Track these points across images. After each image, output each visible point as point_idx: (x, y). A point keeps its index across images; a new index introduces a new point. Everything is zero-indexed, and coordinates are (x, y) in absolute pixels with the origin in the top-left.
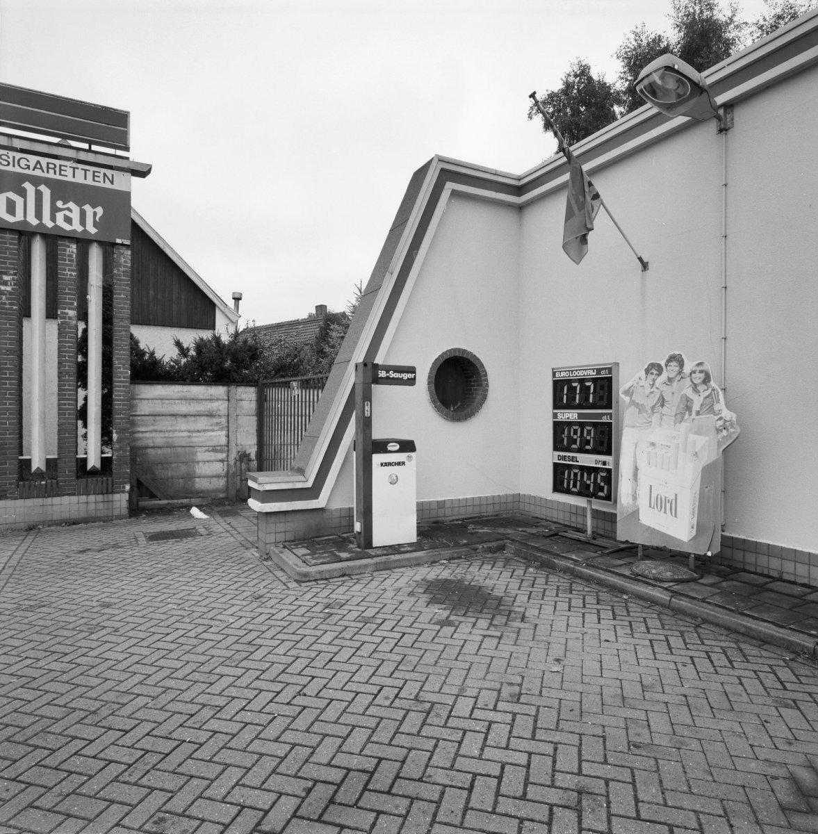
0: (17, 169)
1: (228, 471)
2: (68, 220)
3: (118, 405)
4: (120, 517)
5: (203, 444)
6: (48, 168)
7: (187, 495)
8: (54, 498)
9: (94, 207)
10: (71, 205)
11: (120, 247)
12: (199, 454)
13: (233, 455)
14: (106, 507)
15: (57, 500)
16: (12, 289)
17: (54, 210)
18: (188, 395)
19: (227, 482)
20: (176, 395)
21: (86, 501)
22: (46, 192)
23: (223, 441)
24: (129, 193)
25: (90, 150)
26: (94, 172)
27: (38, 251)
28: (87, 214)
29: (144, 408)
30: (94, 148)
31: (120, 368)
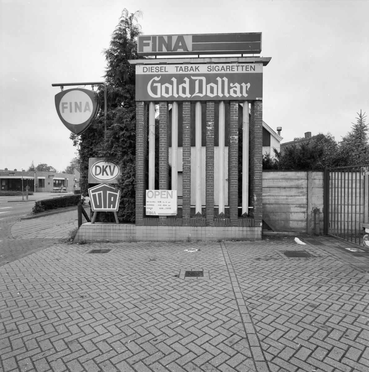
0: (215, 72)
1: (307, 218)
2: (235, 92)
3: (256, 182)
4: (258, 239)
5: (294, 203)
6: (227, 68)
7: (286, 230)
8: (229, 227)
9: (246, 84)
10: (237, 84)
11: (258, 102)
12: (292, 208)
13: (310, 210)
14: (251, 234)
15: (230, 228)
16: (212, 128)
17: (229, 88)
18: (286, 177)
19: (307, 224)
20: (280, 177)
21: (242, 230)
22: (225, 79)
23: (305, 201)
24: (262, 73)
25: (242, 57)
26: (246, 66)
27: (198, 108)
28: (243, 87)
29: (265, 184)
30: (244, 55)
31: (257, 163)
